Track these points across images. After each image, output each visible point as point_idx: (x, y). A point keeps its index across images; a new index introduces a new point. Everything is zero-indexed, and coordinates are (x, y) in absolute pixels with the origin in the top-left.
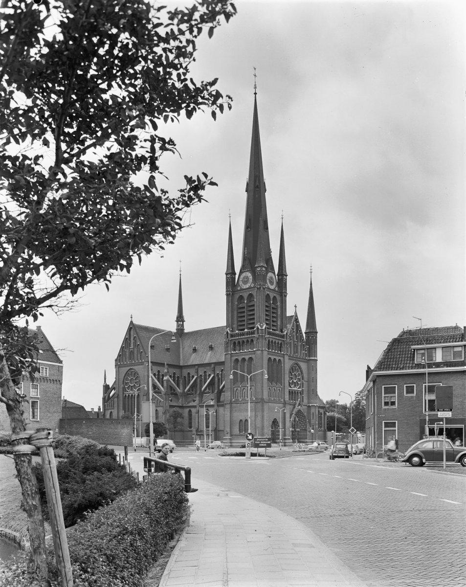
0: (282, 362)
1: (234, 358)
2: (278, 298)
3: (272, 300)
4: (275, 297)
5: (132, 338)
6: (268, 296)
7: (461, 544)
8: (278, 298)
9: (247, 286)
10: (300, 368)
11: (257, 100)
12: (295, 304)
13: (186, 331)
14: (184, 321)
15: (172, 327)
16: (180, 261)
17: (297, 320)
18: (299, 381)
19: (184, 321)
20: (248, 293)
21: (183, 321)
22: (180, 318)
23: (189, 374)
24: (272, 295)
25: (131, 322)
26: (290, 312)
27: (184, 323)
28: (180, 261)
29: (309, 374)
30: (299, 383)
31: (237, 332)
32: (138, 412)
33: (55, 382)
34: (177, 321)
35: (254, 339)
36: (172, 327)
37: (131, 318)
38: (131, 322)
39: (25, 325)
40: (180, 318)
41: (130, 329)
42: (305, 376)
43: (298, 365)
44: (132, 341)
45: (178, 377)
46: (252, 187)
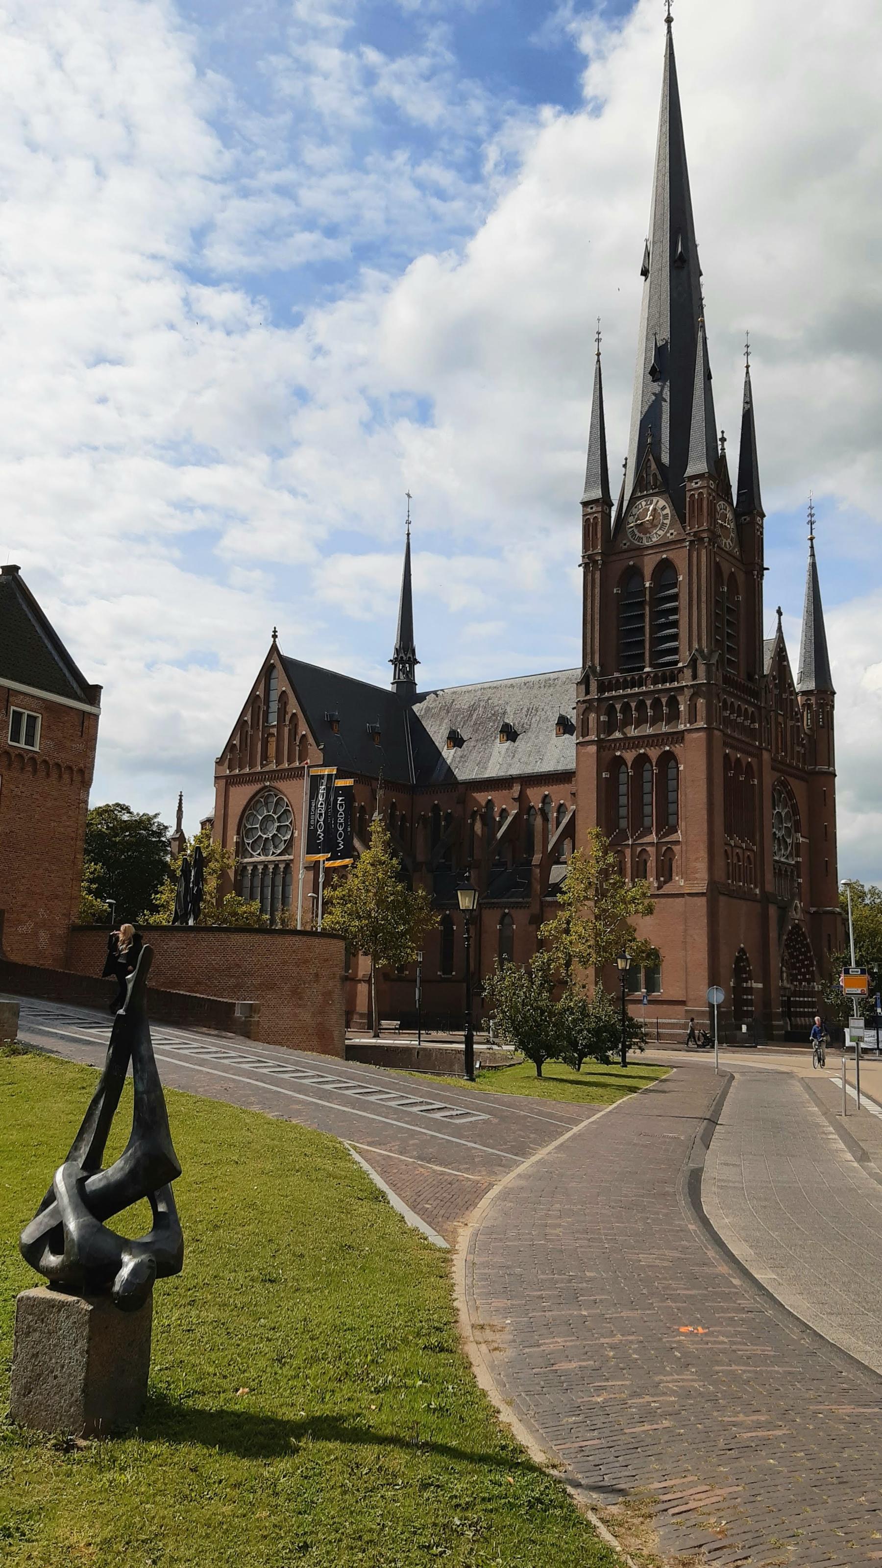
0: (755, 768)
2: (741, 578)
3: (726, 582)
5: (274, 696)
7: (71, 1117)
8: (741, 578)
10: (791, 795)
11: (674, 37)
12: (781, 613)
14: (416, 662)
16: (409, 496)
18: (789, 837)
19: (416, 662)
20: (657, 558)
22: (405, 657)
23: (436, 809)
25: (274, 648)
26: (769, 633)
27: (417, 667)
28: (409, 496)
30: (789, 841)
31: (616, 675)
33: (66, 776)
35: (678, 749)
37: (275, 636)
38: (274, 648)
40: (405, 657)
41: (267, 671)
42: (803, 817)
43: (785, 787)
44: (274, 706)
45: (403, 818)
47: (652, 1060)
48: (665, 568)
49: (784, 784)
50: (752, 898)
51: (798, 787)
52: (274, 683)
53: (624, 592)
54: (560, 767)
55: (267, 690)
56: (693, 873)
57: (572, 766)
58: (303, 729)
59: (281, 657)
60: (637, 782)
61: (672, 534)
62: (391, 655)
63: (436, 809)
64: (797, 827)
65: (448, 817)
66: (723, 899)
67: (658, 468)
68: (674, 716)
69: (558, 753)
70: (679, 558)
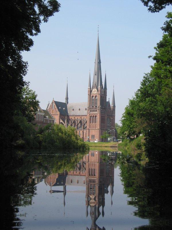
8: (104, 96)
22: (67, 99)
26: (107, 100)
40: (67, 99)
48: (96, 96)
56: (98, 127)
58: (57, 110)
70: (97, 95)
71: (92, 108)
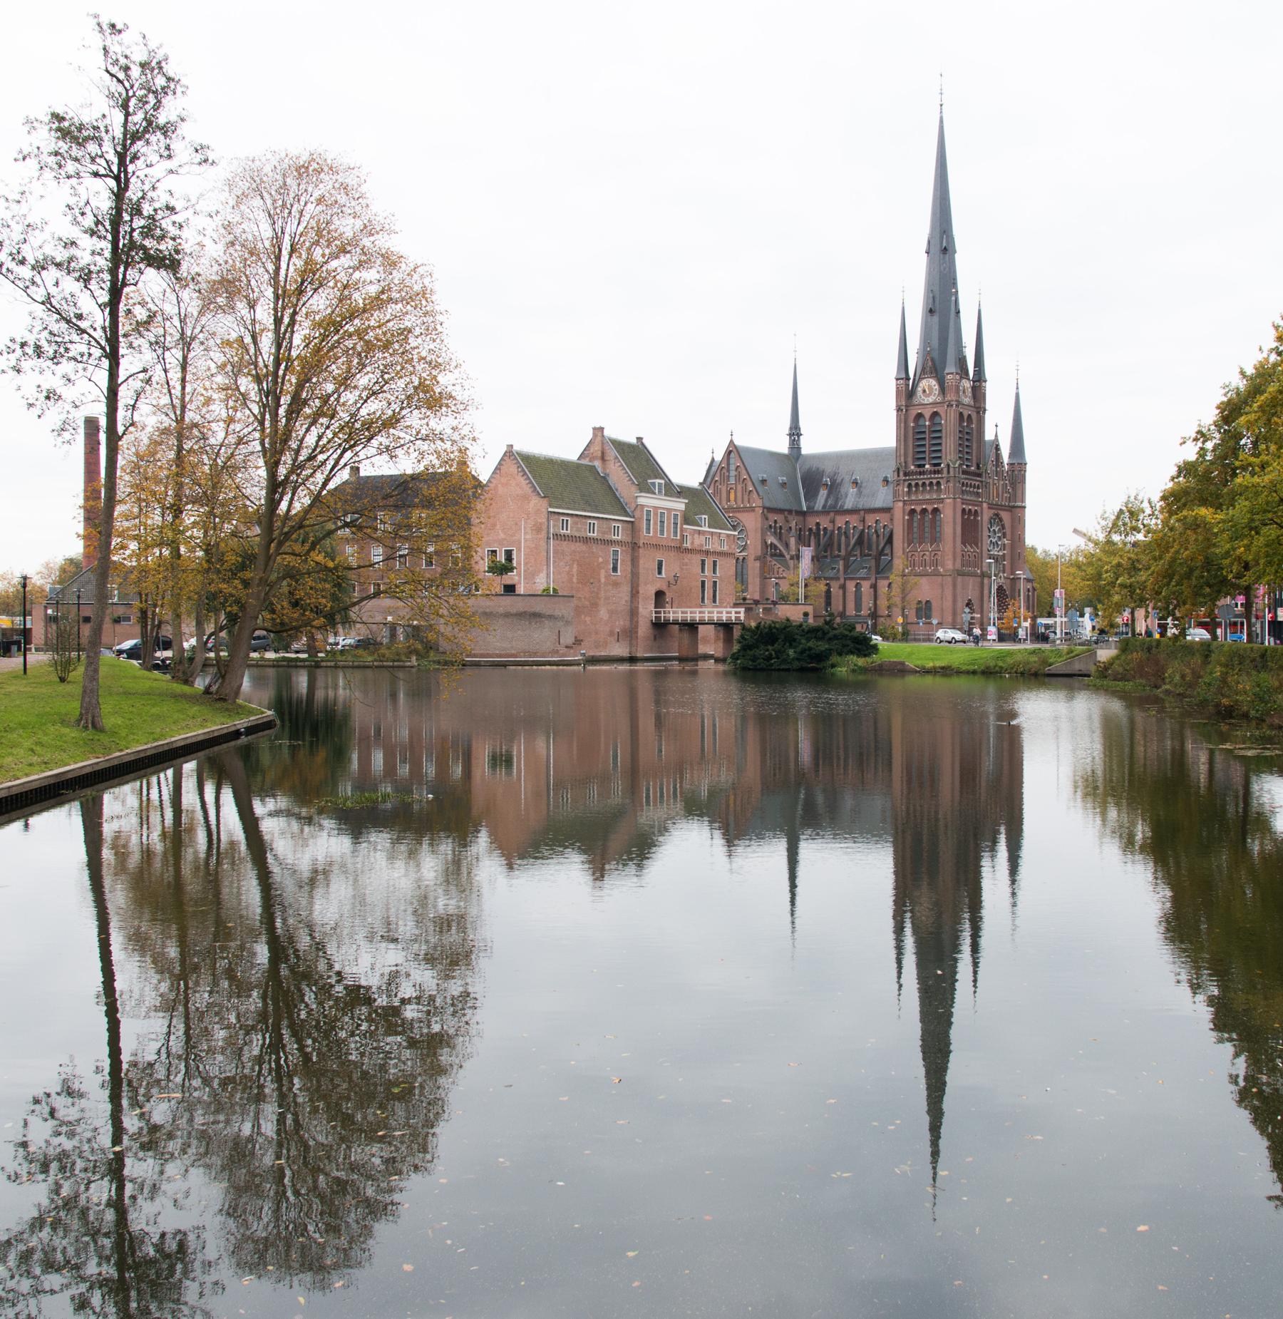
1: (908, 508)
2: (974, 416)
4: (969, 416)
5: (732, 467)
6: (961, 414)
8: (974, 416)
9: (931, 400)
10: (1001, 520)
12: (997, 426)
13: (804, 452)
15: (783, 447)
17: (997, 448)
21: (799, 435)
22: (795, 432)
23: (818, 524)
24: (966, 414)
25: (731, 442)
26: (989, 436)
29: (1013, 527)
32: (975, 948)
34: (790, 435)
36: (783, 447)
38: (731, 442)
39: (192, 1170)
40: (795, 432)
41: (729, 453)
42: (1008, 530)
44: (733, 473)
46: (936, 249)
47: (525, 653)
49: (997, 515)
50: (975, 575)
51: (1005, 516)
52: (732, 461)
53: (919, 432)
54: (885, 505)
55: (728, 464)
57: (890, 505)
59: (735, 446)
60: (922, 521)
61: (939, 399)
62: (787, 432)
63: (818, 524)
64: (1004, 535)
65: (825, 529)
66: (960, 578)
67: (933, 365)
68: (939, 490)
69: (882, 497)
71: (916, 473)
